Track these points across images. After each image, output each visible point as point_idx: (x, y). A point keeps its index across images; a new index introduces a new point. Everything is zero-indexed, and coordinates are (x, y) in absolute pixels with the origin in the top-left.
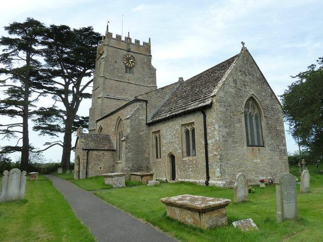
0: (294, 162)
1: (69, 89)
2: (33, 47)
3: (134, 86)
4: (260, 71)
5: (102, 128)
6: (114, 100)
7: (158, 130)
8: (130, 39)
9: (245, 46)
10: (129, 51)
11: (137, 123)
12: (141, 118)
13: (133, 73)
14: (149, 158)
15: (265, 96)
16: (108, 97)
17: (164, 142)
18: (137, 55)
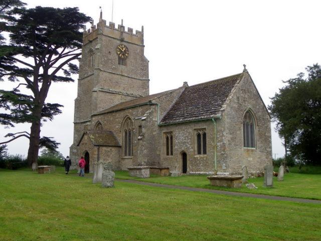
0: (277, 164)
3: (127, 79)
4: (256, 89)
6: (108, 94)
7: (169, 131)
8: (124, 27)
9: (247, 68)
10: (122, 40)
11: (151, 124)
12: (154, 119)
13: (125, 65)
15: (258, 109)
17: (177, 141)
18: (130, 45)
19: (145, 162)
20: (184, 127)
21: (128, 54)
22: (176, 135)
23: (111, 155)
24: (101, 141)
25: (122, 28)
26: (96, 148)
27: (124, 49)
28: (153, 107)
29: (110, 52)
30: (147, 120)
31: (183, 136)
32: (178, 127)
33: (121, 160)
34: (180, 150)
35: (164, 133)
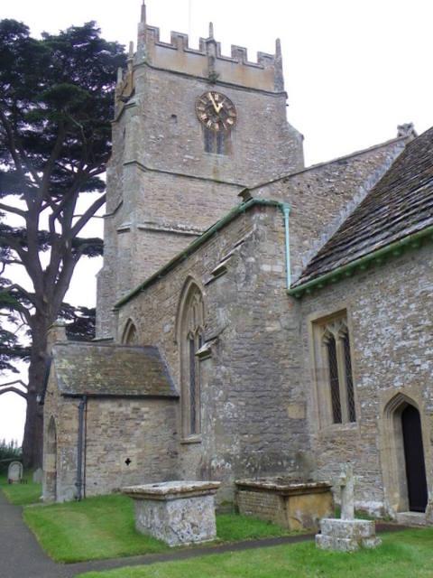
1: (40, 229)
2: (44, 268)
5: (133, 327)
6: (170, 238)
8: (216, 44)
10: (212, 80)
11: (253, 287)
12: (266, 268)
13: (228, 151)
14: (303, 422)
16: (152, 227)
19: (228, 458)
20: (392, 278)
21: (234, 119)
22: (364, 323)
23: (138, 433)
24: (97, 381)
25: (212, 46)
26: (72, 407)
27: (221, 105)
28: (262, 216)
29: (174, 116)
30: (230, 270)
31: (393, 321)
32: (261, 200)
33: (178, 448)
34: (386, 394)
35: (315, 323)
